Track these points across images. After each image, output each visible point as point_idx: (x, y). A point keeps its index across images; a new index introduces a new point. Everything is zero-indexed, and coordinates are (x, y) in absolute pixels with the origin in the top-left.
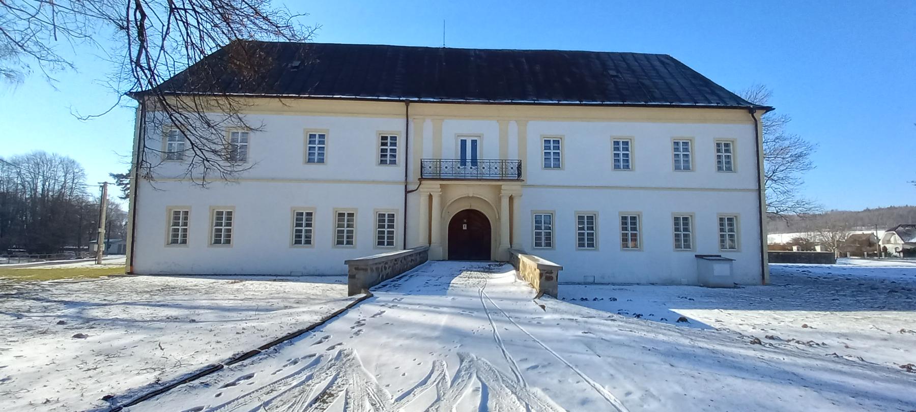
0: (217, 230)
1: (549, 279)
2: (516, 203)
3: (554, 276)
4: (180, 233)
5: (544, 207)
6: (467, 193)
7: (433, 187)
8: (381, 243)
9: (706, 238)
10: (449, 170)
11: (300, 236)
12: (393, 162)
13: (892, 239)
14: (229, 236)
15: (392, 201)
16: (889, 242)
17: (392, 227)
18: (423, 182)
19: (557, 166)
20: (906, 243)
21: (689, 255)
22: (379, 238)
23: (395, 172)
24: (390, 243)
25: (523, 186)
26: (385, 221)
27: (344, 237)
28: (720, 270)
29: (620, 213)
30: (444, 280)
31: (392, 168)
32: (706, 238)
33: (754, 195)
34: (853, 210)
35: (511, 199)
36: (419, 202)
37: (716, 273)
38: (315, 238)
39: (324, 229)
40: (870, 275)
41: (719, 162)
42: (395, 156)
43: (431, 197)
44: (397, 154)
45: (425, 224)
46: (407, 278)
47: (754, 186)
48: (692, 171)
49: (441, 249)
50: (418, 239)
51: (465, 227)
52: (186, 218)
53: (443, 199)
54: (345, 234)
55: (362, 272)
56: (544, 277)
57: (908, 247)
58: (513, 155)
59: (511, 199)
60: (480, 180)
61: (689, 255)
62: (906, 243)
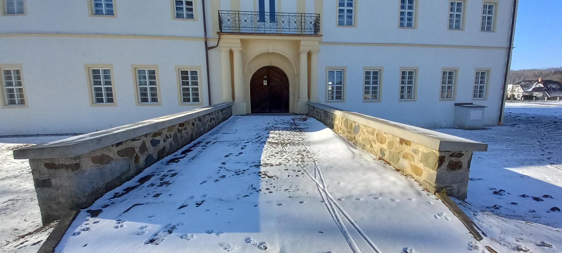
0: (96, 89)
1: (455, 166)
2: (314, 57)
3: (464, 160)
4: (15, 93)
5: (337, 63)
6: (268, 49)
7: (232, 42)
8: (186, 100)
9: (464, 90)
10: (248, 24)
11: (146, 94)
12: (191, 16)
13: (516, 89)
14: (197, 95)
15: (194, 59)
16: (514, 91)
17: (196, 84)
18: (222, 36)
19: (350, 24)
20: (524, 92)
21: (450, 104)
22: (184, 94)
23: (194, 27)
24: (196, 100)
25: (320, 43)
26: (187, 77)
27: (148, 95)
28: (474, 115)
29: (401, 67)
30: (248, 154)
31: (190, 22)
32: (464, 90)
33: (504, 52)
34: (516, 70)
35: (309, 55)
36: (220, 59)
37: (471, 118)
38: (117, 96)
39: (125, 88)
40: (539, 113)
41: (402, 19)
42: (191, 10)
43: (231, 53)
44: (194, 7)
45: (228, 82)
46: (199, 148)
47: (505, 44)
48: (462, 30)
49: (245, 104)
50: (222, 96)
51: (265, 83)
52: (19, 78)
53: (243, 54)
54: (191, 92)
55: (63, 173)
56: (446, 164)
57: (525, 94)
58: (310, 9)
59: (309, 55)
60: (280, 35)
61: (451, 103)
62: (524, 92)
